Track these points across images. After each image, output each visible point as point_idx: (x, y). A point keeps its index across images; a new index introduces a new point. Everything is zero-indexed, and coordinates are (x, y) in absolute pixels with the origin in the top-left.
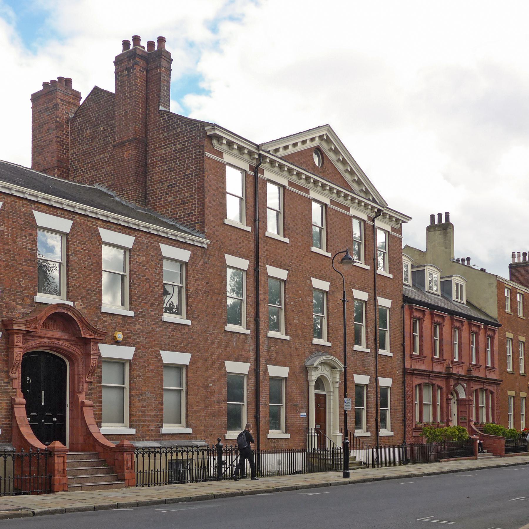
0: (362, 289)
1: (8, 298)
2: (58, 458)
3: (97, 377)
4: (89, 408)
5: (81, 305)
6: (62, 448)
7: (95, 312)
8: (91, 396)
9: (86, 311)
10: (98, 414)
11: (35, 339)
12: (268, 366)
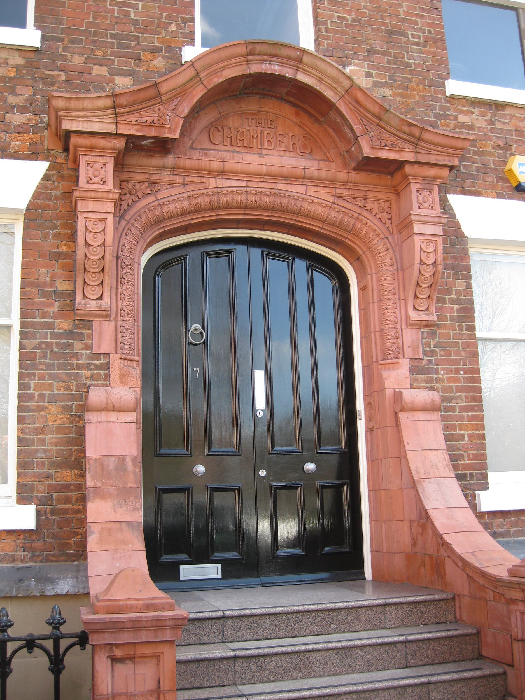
1: (76, 57)
2: (119, 667)
3: (456, 307)
4: (422, 416)
5: (368, 75)
6: (149, 607)
7: (423, 98)
8: (437, 372)
9: (388, 92)
10: (471, 437)
11: (188, 179)
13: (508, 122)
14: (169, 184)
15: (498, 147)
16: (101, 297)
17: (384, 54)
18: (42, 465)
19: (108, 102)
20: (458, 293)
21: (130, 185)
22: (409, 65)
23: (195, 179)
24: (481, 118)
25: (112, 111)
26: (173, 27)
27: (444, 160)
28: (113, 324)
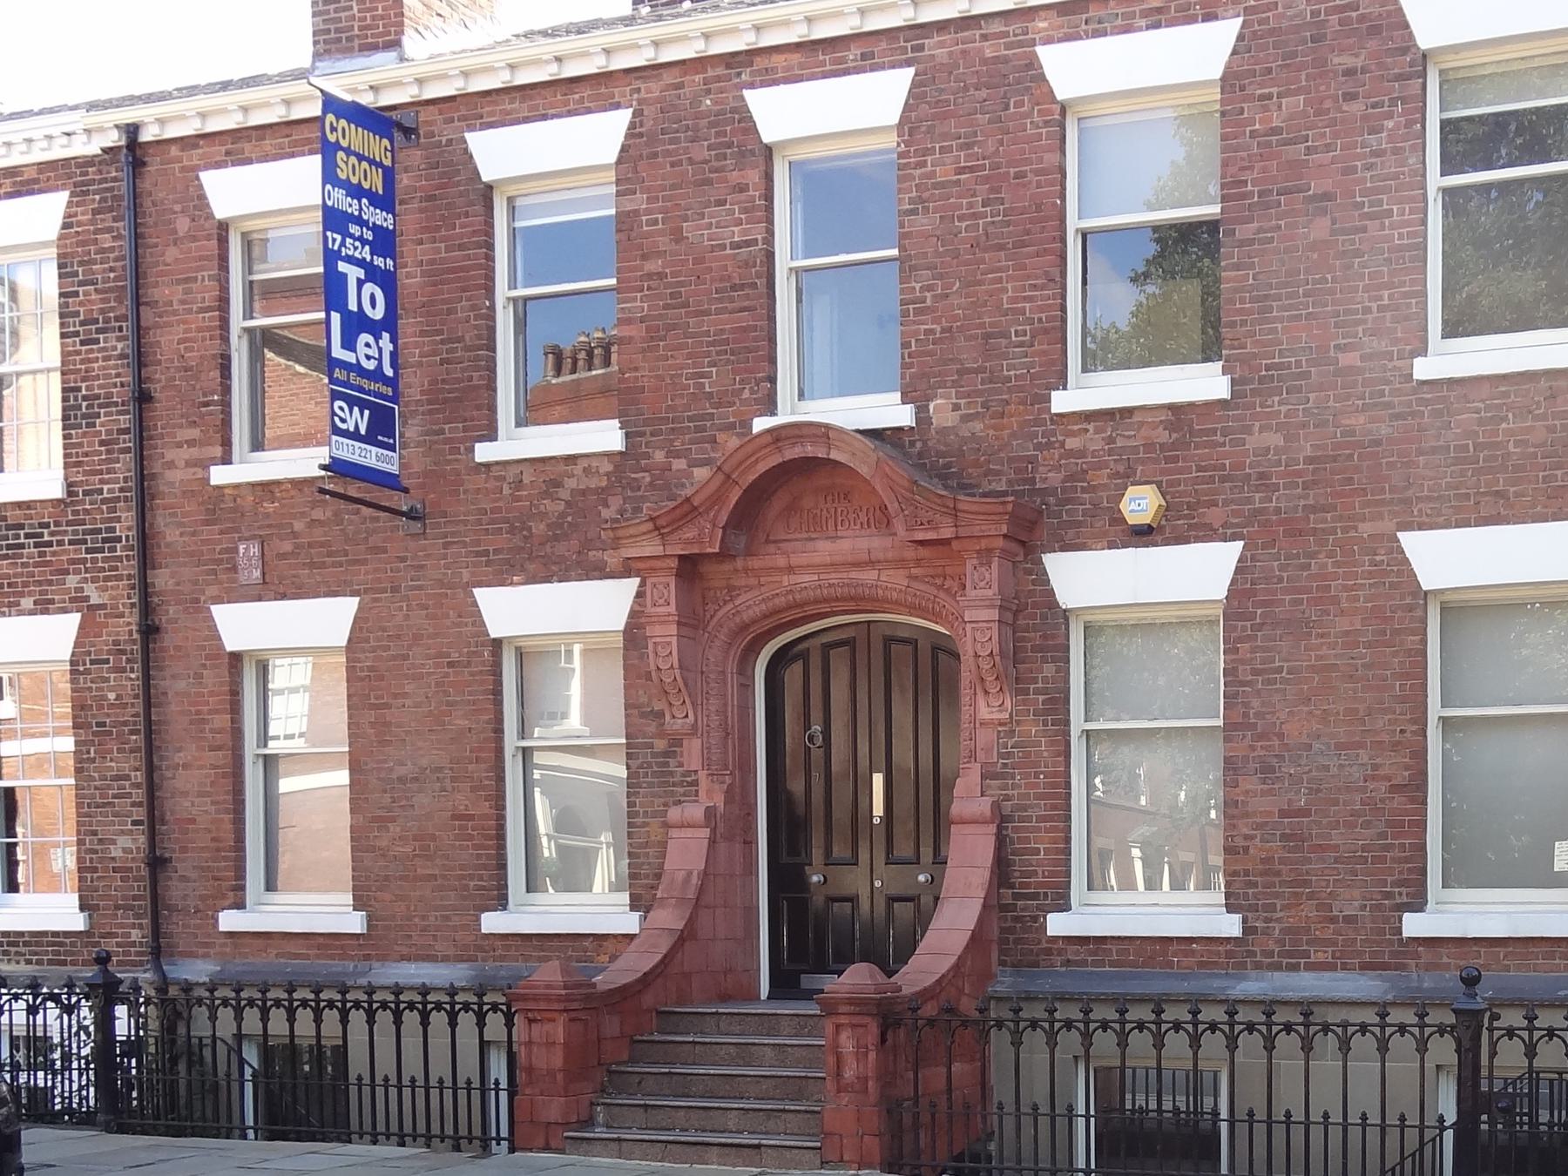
1: (657, 452)
3: (1041, 698)
13: (1135, 436)
14: (747, 586)
15: (1117, 475)
16: (687, 716)
17: (977, 371)
18: (647, 876)
19: (650, 526)
20: (1046, 680)
21: (712, 592)
22: (1009, 379)
23: (770, 579)
24: (1097, 436)
25: (657, 532)
26: (746, 394)
27: (990, 530)
28: (700, 740)
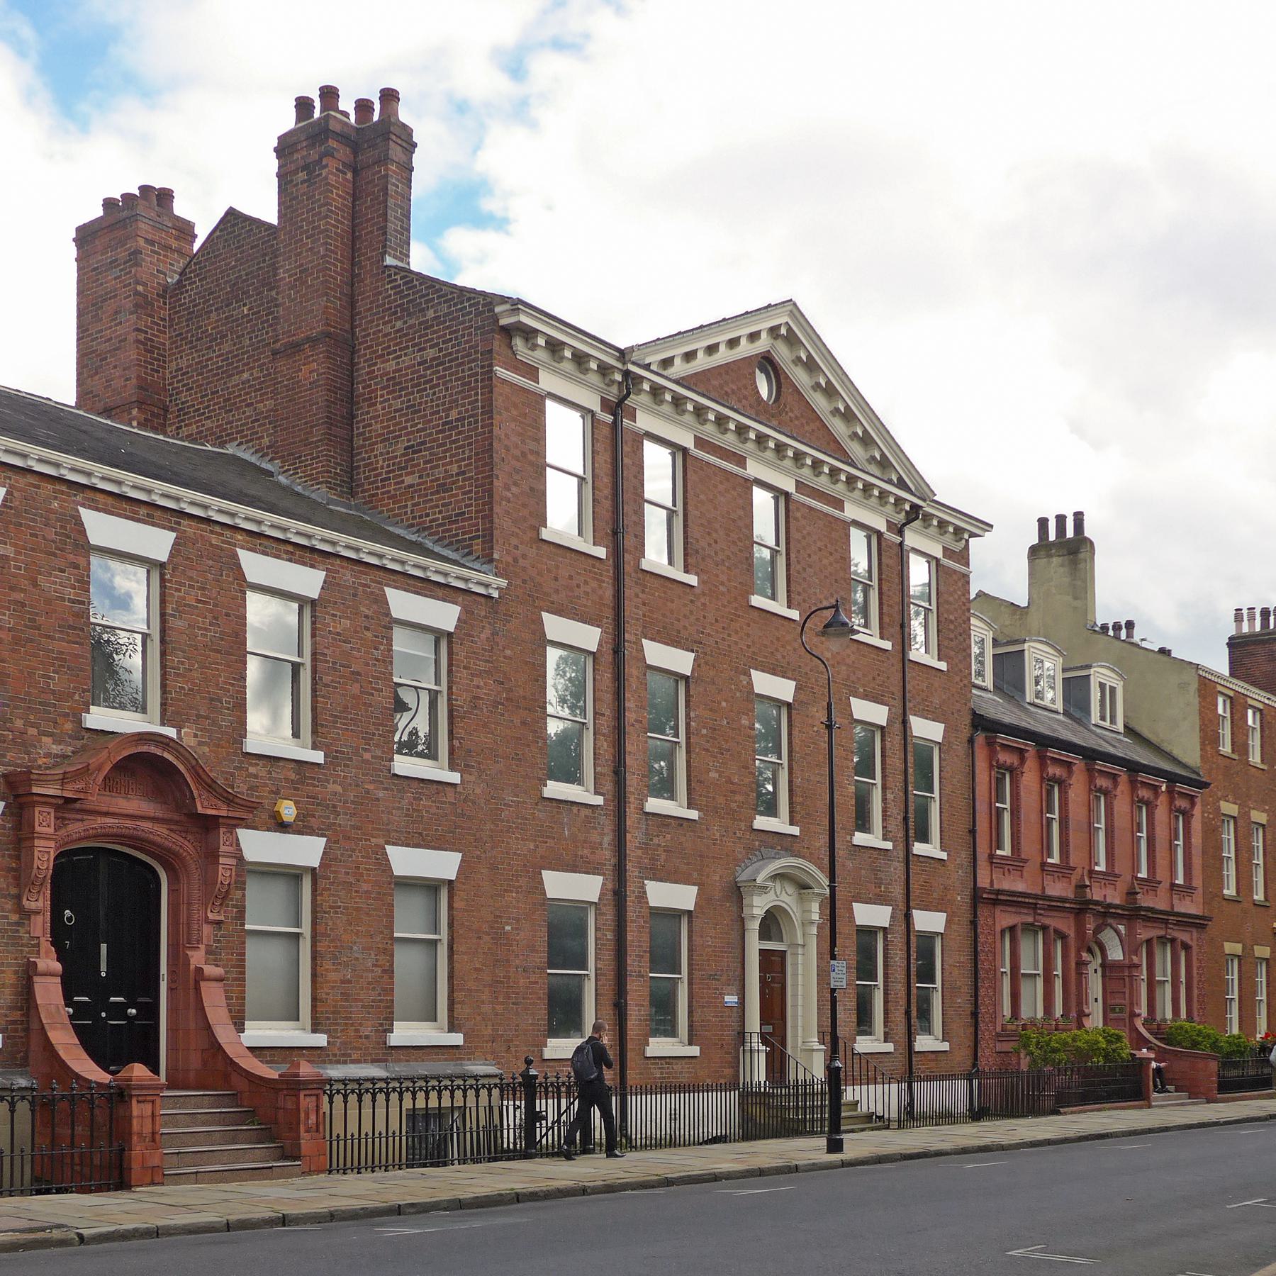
0: (873, 697)
1: (18, 720)
2: (139, 1104)
3: (235, 910)
4: (214, 984)
5: (196, 736)
6: (151, 1080)
7: (228, 753)
8: (221, 955)
9: (206, 749)
10: (237, 998)
11: (85, 817)
12: (646, 882)
